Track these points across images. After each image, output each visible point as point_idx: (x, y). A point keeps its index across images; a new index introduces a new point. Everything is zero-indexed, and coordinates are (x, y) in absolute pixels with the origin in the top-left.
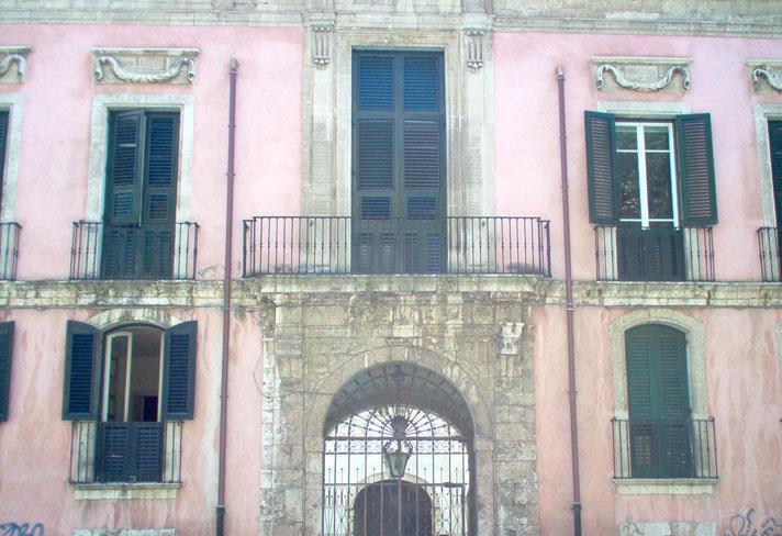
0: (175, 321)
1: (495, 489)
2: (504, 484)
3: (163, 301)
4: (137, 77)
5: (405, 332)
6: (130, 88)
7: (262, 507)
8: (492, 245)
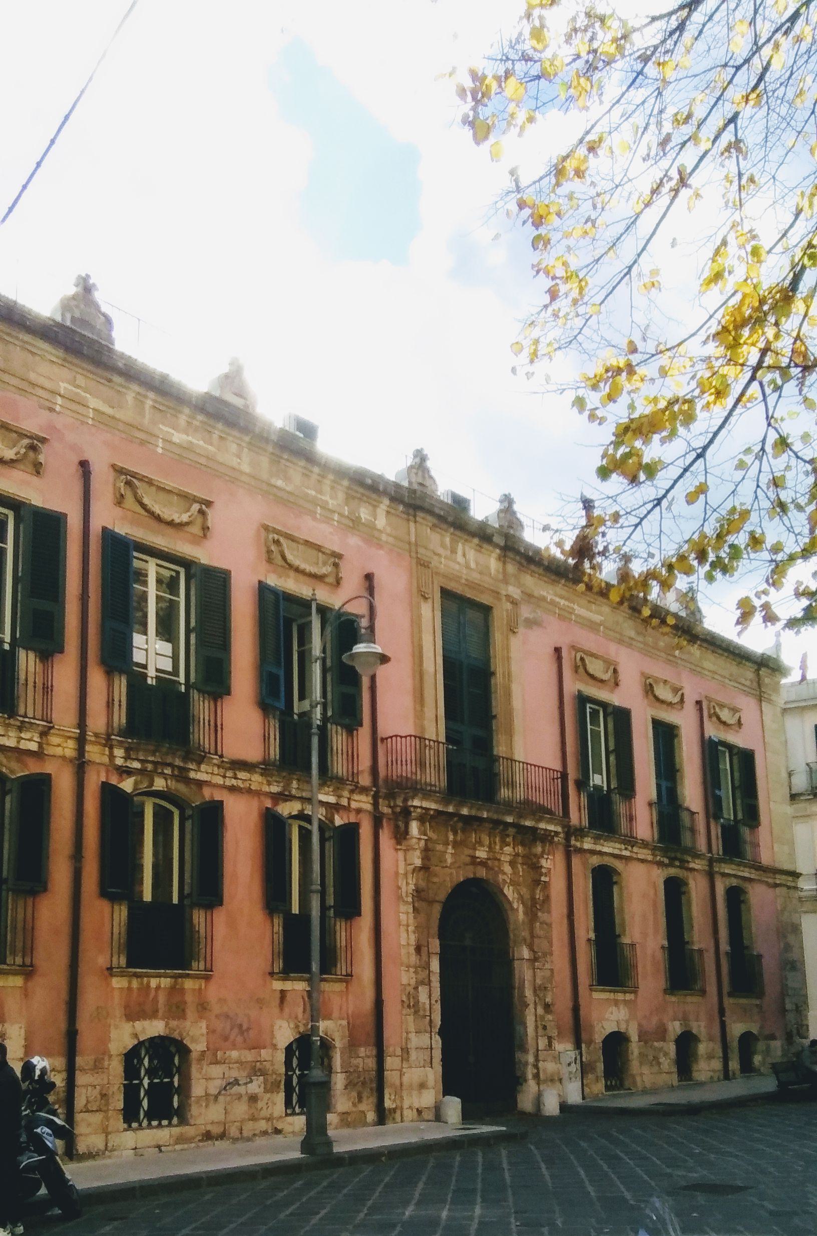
0: (338, 821)
1: (535, 991)
2: (540, 987)
3: (332, 799)
4: (303, 566)
5: (482, 854)
6: (292, 573)
7: (403, 1001)
8: (404, 763)
